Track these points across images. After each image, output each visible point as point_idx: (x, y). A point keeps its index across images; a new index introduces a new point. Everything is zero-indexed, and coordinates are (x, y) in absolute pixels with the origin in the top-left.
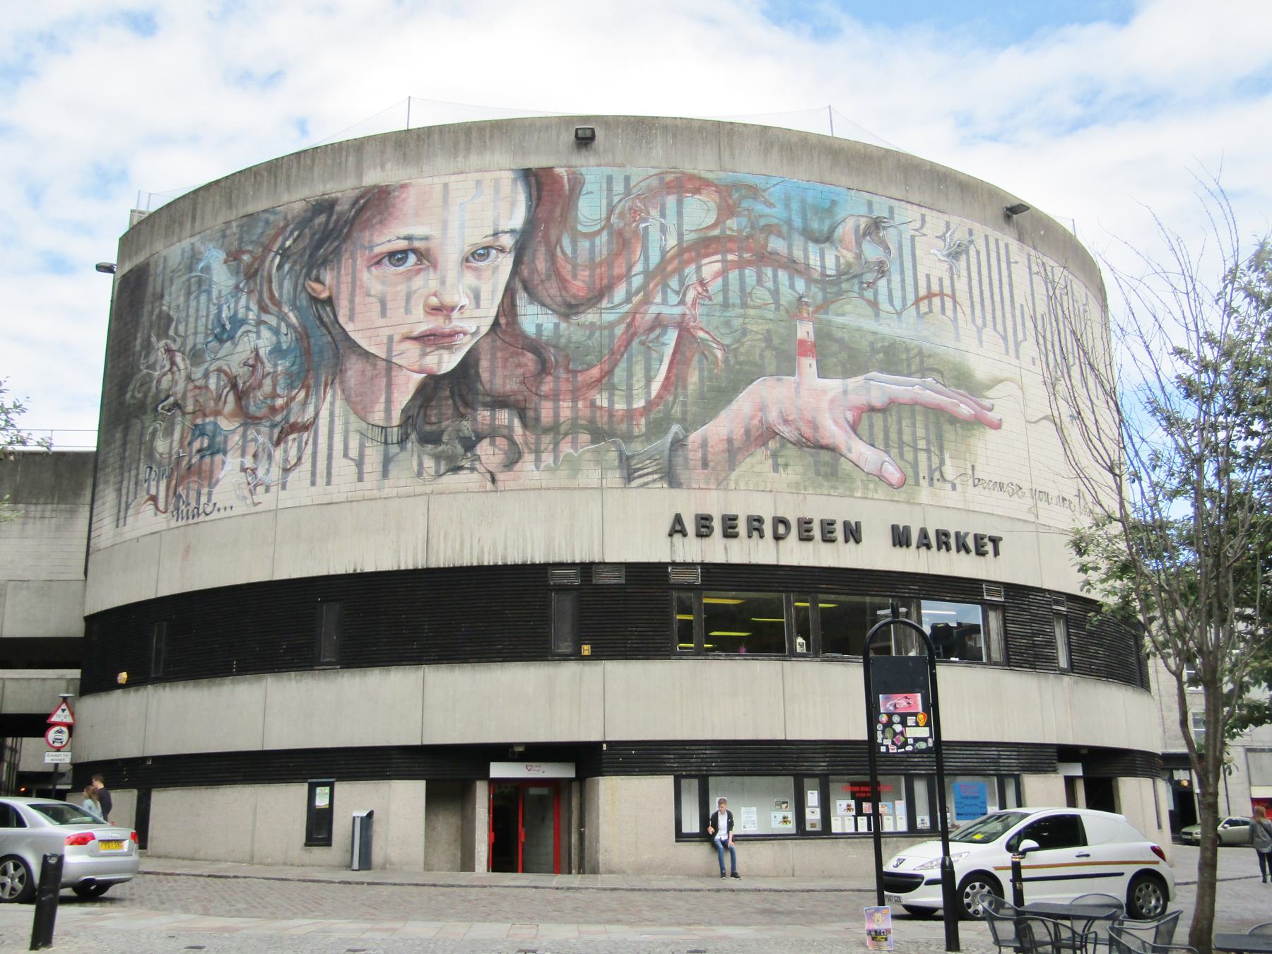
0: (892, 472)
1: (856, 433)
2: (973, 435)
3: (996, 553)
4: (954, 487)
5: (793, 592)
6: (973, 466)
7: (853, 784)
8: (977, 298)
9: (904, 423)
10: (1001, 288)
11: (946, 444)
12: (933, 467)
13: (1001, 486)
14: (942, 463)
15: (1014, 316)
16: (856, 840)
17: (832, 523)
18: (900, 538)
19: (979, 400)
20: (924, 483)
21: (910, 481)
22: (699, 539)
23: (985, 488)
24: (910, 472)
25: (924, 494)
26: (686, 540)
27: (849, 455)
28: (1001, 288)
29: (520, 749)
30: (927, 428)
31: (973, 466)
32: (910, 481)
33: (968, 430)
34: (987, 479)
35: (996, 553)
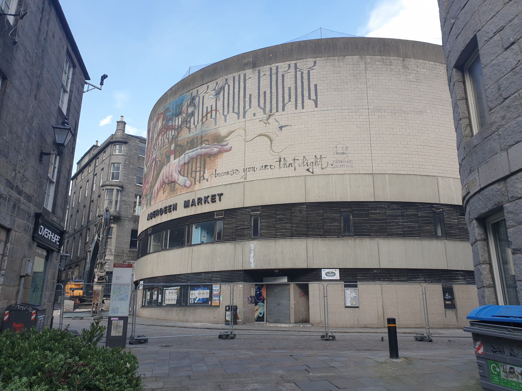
0: (188, 183)
1: (180, 174)
2: (218, 158)
3: (220, 200)
4: (207, 181)
5: (193, 223)
6: (216, 170)
7: (256, 285)
8: (226, 104)
9: (194, 164)
10: (228, 97)
11: (206, 166)
12: (201, 176)
13: (228, 173)
14: (204, 173)
15: (244, 102)
16: (423, 314)
17: (215, 195)
18: (187, 205)
19: (222, 144)
20: (197, 183)
21: (193, 184)
22: (213, 203)
23: (220, 176)
24: (193, 181)
25: (197, 187)
26: (196, 207)
27: (178, 182)
28: (228, 97)
29: (278, 271)
30: (200, 163)
31: (216, 170)
32: (193, 184)
33: (215, 157)
34: (221, 173)
35: (220, 200)
